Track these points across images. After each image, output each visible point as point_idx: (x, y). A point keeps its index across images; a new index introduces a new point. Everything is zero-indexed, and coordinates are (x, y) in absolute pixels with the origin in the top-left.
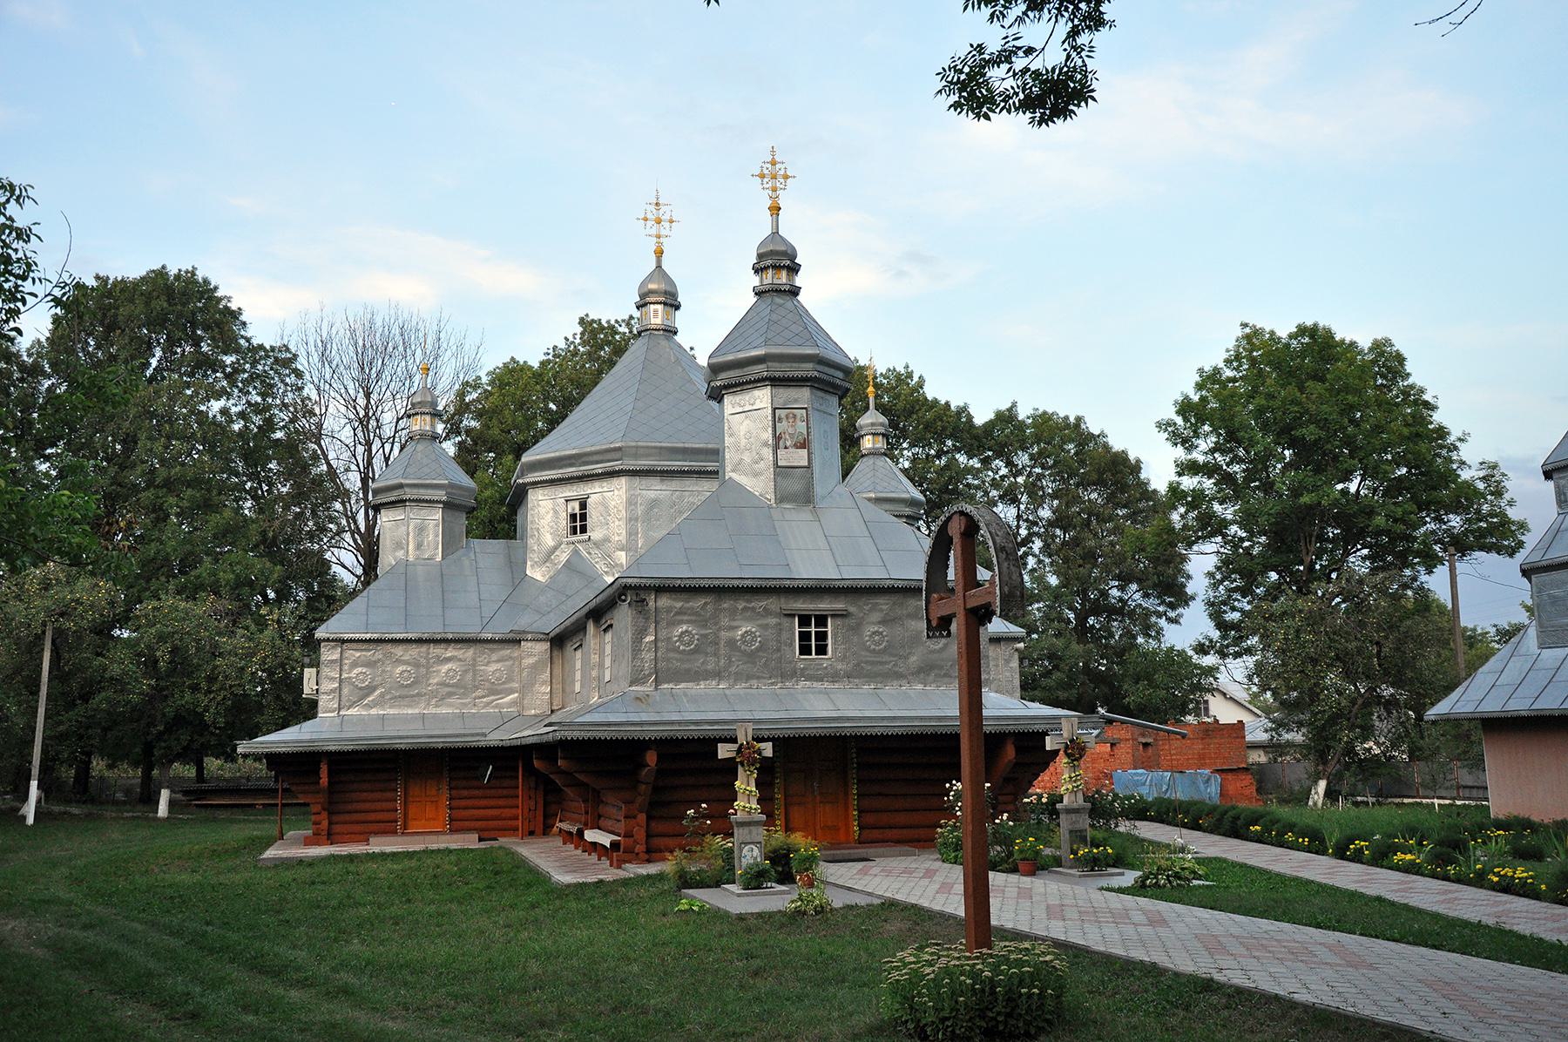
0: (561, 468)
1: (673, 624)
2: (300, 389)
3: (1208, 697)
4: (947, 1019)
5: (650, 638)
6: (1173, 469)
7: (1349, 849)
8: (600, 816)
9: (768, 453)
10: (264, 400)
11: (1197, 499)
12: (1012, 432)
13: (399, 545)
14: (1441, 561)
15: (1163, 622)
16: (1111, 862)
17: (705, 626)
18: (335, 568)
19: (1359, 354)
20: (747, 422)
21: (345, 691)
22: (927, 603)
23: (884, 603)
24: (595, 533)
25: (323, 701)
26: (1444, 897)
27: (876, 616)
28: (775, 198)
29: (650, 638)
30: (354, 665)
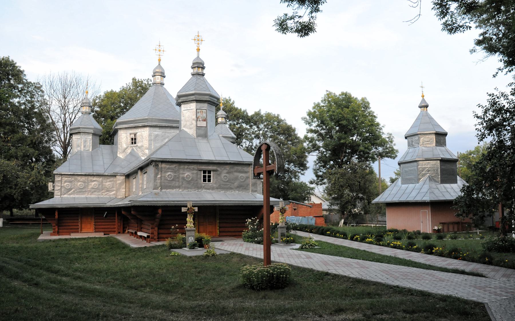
0: (128, 124)
1: (166, 172)
2: (43, 96)
3: (312, 196)
4: (260, 284)
5: (159, 176)
6: (306, 131)
7: (354, 238)
8: (142, 228)
9: (194, 122)
10: (31, 99)
11: (312, 140)
12: (259, 118)
13: (78, 146)
14: (376, 160)
15: (300, 174)
16: (292, 242)
17: (175, 173)
18: (54, 152)
19: (358, 101)
20: (189, 113)
21: (63, 190)
22: (254, 168)
23: (228, 167)
24: (139, 144)
25: (56, 193)
26: (380, 250)
27: (225, 171)
28: (198, 47)
29: (159, 176)
30: (65, 182)
